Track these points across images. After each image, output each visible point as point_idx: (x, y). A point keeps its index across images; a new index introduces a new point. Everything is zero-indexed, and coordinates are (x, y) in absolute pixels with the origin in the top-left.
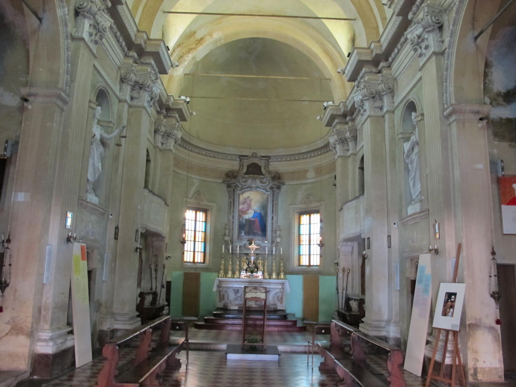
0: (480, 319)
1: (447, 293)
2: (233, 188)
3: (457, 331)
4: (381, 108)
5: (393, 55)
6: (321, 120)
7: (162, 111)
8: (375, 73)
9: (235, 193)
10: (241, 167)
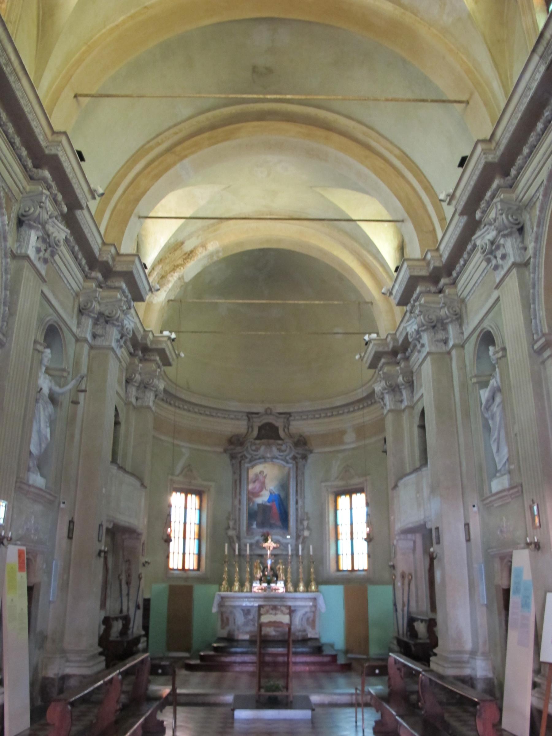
2: (239, 459)
5: (458, 268)
6: (362, 360)
7: (136, 352)
8: (434, 293)
9: (242, 466)
10: (250, 430)
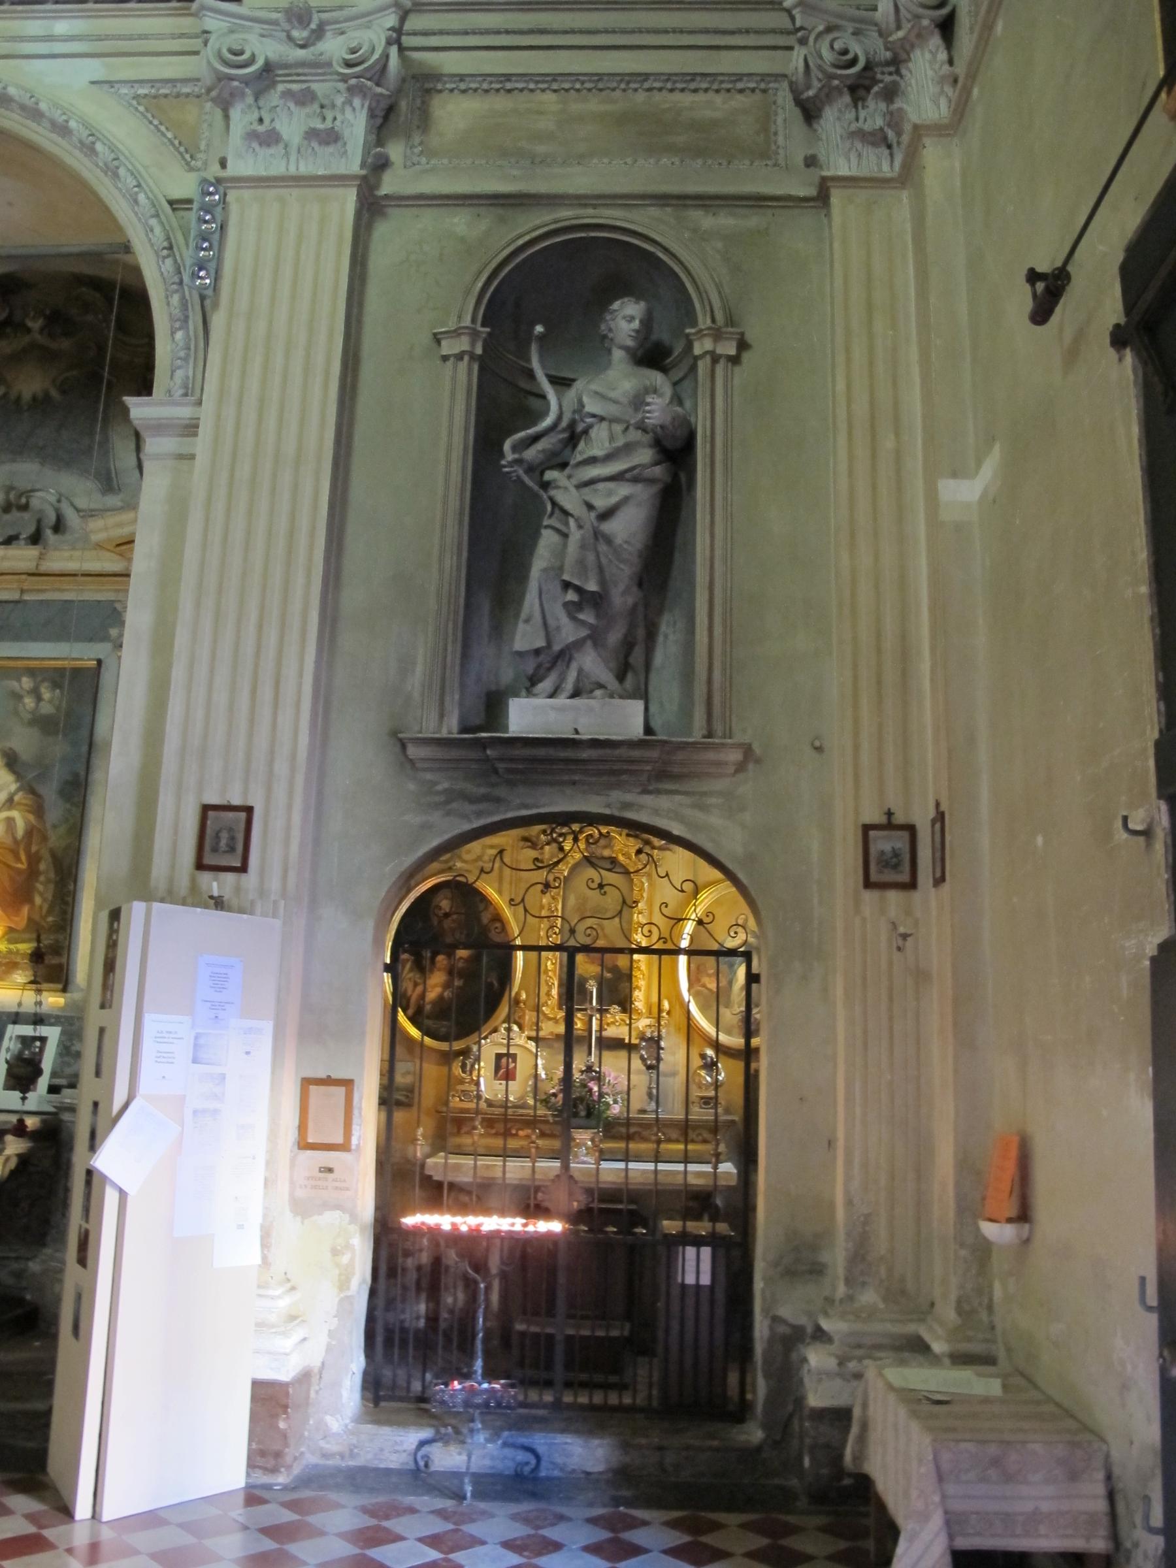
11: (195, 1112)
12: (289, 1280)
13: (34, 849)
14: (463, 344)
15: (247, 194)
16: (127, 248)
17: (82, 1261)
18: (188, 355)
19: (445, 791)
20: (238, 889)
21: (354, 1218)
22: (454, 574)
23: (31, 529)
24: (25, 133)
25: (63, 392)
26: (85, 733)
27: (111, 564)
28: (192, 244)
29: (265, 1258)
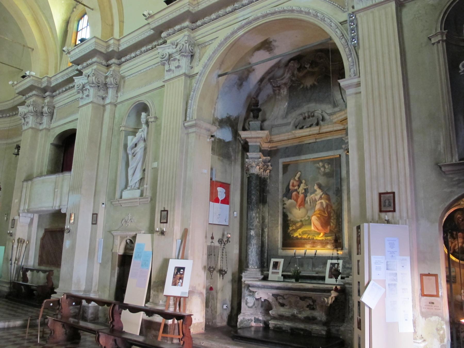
0: (195, 287)
1: (176, 267)
3: (186, 297)
4: (103, 99)
5: (128, 57)
6: (13, 86)
8: (104, 65)
11: (389, 285)
12: (423, 338)
13: (329, 210)
14: (439, 38)
15: (362, 14)
16: (330, 39)
17: (359, 327)
18: (354, 64)
19: (457, 180)
20: (393, 217)
21: (443, 319)
22: (449, 111)
23: (316, 122)
24: (299, 17)
25: (318, 82)
26: (339, 176)
27: (340, 127)
28: (349, 33)
29: (414, 330)
